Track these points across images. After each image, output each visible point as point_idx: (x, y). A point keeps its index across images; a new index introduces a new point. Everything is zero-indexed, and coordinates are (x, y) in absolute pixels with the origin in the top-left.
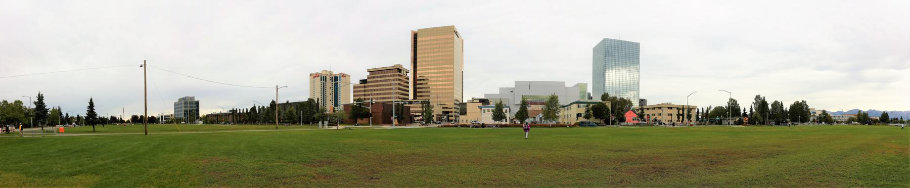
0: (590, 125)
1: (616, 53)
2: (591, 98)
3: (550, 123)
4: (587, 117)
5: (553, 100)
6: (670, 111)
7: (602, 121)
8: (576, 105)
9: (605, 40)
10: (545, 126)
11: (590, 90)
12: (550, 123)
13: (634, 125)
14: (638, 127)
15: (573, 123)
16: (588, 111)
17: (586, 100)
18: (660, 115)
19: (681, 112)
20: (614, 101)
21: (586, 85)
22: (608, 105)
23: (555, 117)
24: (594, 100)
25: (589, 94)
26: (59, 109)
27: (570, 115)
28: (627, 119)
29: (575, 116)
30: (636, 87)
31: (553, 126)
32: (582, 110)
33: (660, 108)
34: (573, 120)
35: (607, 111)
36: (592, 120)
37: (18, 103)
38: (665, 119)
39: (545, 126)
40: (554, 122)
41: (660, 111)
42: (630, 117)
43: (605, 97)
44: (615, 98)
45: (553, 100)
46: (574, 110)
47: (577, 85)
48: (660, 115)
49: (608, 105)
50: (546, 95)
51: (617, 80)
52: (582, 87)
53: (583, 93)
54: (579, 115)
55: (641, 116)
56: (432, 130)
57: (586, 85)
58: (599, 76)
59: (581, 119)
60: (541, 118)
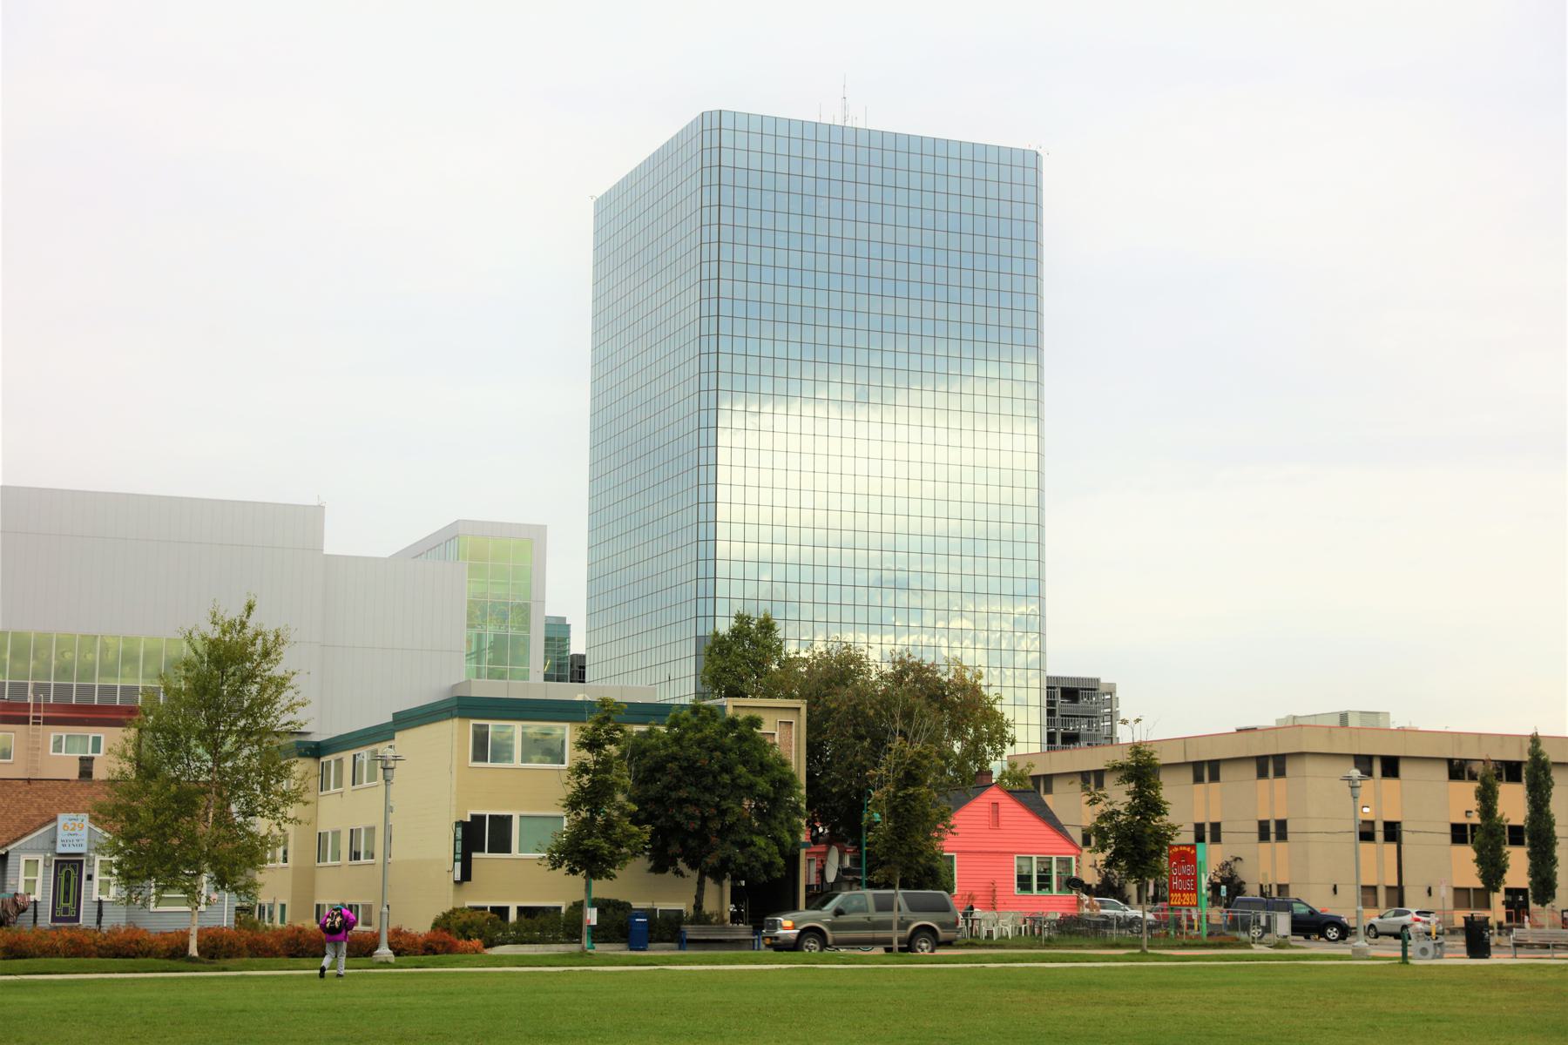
0: (622, 927)
1: (826, 246)
2: (577, 670)
3: (168, 913)
4: (582, 855)
5: (223, 687)
6: (1381, 799)
7: (719, 900)
8: (456, 733)
9: (711, 135)
10: (128, 950)
11: (565, 593)
12: (168, 913)
13: (1035, 935)
14: (617, 969)
15: (421, 926)
16: (591, 794)
17: (533, 684)
18: (1273, 831)
19: (1513, 804)
20: (832, 689)
21: (532, 540)
22: (784, 732)
23: (236, 861)
24: (610, 681)
25: (557, 635)
26: (767, 626)
27: (387, 832)
28: (964, 877)
29: (445, 846)
30: (1015, 567)
31: (217, 950)
32: (535, 785)
33: (1271, 765)
34: (422, 890)
35: (769, 791)
36: (635, 886)
37: (312, 517)
38: (1324, 871)
39: (128, 950)
40: (216, 909)
41: (1270, 798)
42: (981, 847)
43: (741, 656)
44: (841, 671)
45: (223, 687)
46: (434, 784)
47: (447, 544)
48: (1273, 831)
49: (784, 732)
50: (146, 629)
51: (841, 512)
52: (484, 562)
53: (503, 618)
54: (480, 836)
55: (1137, 846)
56: (1500, 979)
57: (532, 540)
58: (654, 465)
59: (522, 878)
60: (69, 869)
